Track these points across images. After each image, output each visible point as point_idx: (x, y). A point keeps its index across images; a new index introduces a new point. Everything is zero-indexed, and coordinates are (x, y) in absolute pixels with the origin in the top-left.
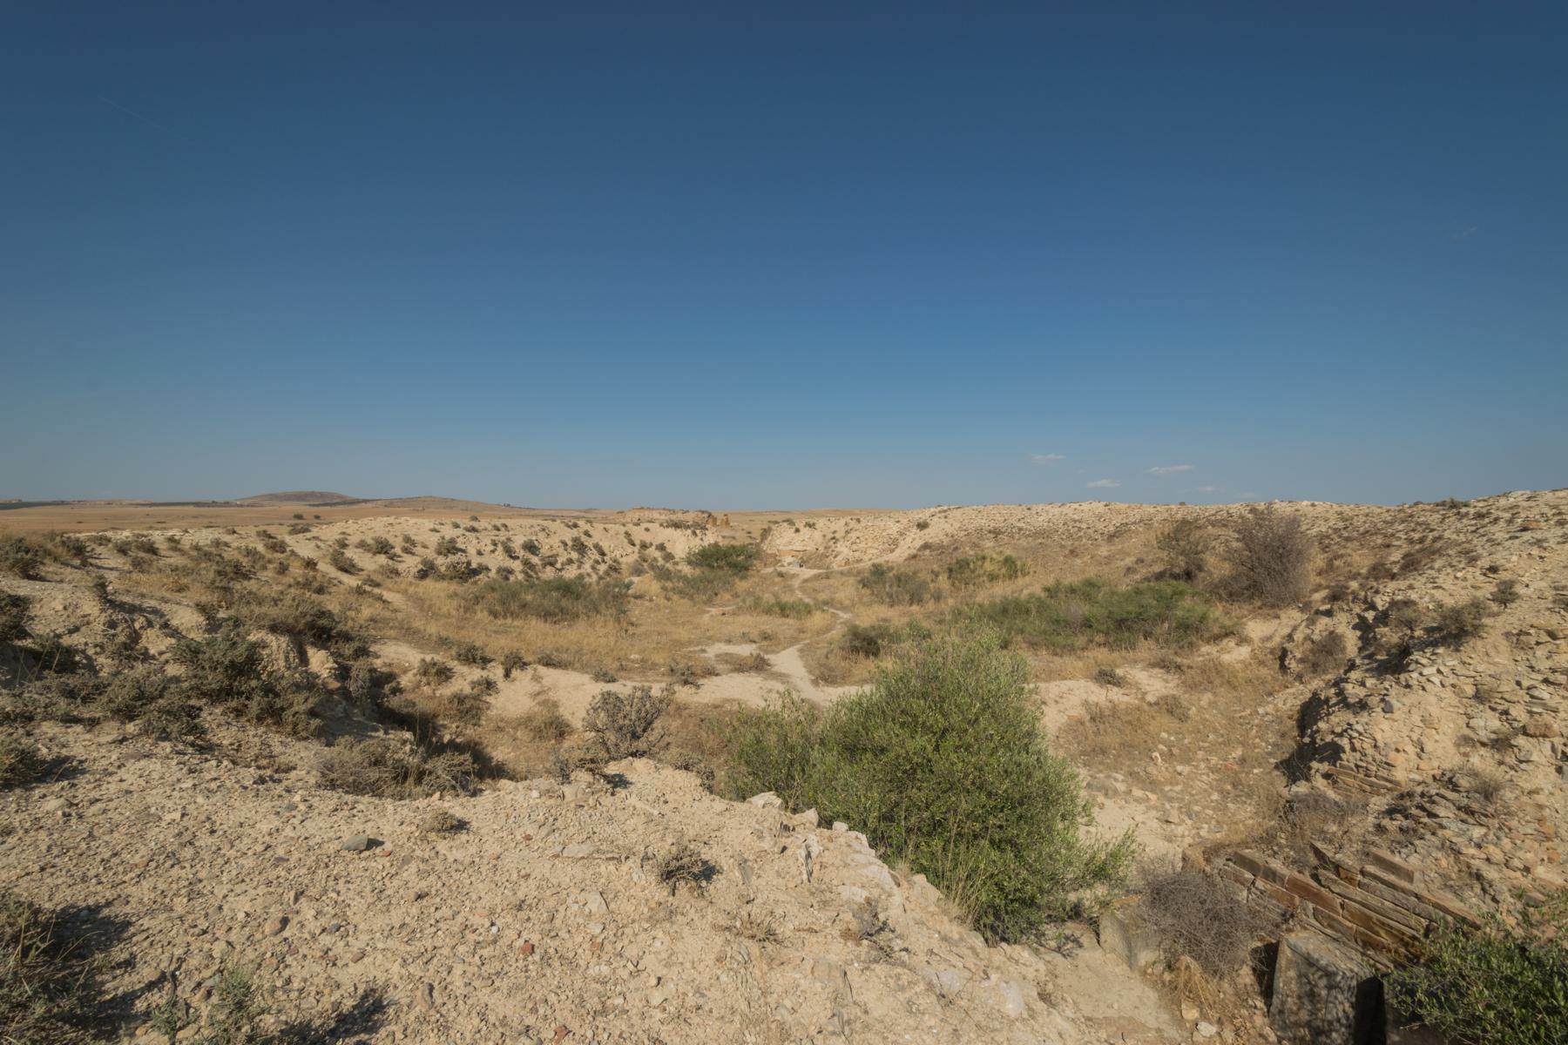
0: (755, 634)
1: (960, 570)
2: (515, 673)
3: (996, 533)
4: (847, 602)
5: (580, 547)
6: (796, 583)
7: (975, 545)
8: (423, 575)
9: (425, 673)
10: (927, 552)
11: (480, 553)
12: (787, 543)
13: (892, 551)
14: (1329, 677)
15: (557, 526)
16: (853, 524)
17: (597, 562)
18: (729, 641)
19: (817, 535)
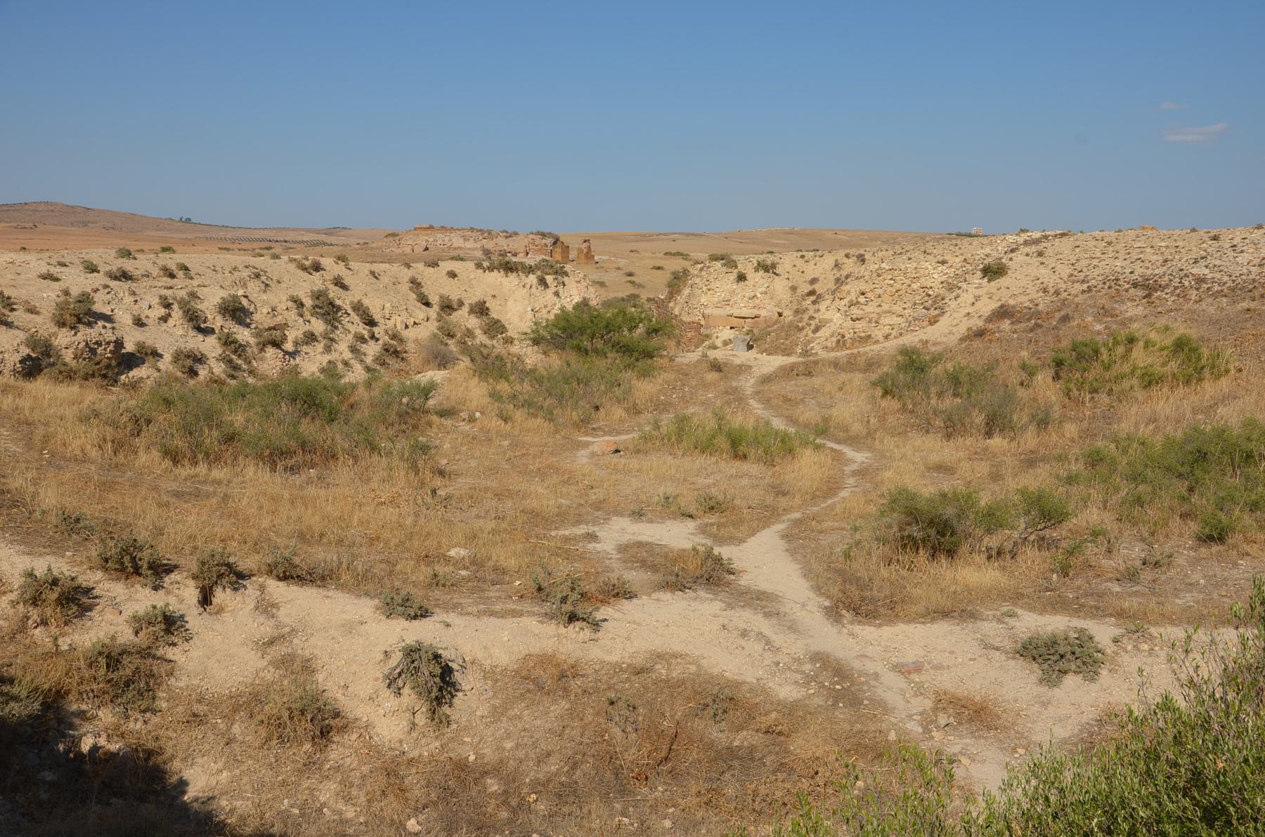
0: (688, 500)
1: (1078, 363)
2: (221, 596)
3: (1149, 287)
4: (857, 428)
5: (328, 310)
6: (748, 384)
7: (1104, 312)
8: (31, 368)
9: (35, 601)
10: (1006, 325)
11: (139, 323)
12: (720, 302)
13: (933, 321)
14: (1056, 408)
15: (281, 268)
16: (850, 265)
17: (362, 339)
18: (638, 515)
19: (780, 286)
